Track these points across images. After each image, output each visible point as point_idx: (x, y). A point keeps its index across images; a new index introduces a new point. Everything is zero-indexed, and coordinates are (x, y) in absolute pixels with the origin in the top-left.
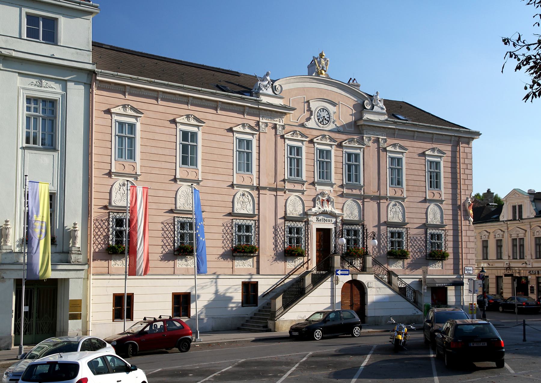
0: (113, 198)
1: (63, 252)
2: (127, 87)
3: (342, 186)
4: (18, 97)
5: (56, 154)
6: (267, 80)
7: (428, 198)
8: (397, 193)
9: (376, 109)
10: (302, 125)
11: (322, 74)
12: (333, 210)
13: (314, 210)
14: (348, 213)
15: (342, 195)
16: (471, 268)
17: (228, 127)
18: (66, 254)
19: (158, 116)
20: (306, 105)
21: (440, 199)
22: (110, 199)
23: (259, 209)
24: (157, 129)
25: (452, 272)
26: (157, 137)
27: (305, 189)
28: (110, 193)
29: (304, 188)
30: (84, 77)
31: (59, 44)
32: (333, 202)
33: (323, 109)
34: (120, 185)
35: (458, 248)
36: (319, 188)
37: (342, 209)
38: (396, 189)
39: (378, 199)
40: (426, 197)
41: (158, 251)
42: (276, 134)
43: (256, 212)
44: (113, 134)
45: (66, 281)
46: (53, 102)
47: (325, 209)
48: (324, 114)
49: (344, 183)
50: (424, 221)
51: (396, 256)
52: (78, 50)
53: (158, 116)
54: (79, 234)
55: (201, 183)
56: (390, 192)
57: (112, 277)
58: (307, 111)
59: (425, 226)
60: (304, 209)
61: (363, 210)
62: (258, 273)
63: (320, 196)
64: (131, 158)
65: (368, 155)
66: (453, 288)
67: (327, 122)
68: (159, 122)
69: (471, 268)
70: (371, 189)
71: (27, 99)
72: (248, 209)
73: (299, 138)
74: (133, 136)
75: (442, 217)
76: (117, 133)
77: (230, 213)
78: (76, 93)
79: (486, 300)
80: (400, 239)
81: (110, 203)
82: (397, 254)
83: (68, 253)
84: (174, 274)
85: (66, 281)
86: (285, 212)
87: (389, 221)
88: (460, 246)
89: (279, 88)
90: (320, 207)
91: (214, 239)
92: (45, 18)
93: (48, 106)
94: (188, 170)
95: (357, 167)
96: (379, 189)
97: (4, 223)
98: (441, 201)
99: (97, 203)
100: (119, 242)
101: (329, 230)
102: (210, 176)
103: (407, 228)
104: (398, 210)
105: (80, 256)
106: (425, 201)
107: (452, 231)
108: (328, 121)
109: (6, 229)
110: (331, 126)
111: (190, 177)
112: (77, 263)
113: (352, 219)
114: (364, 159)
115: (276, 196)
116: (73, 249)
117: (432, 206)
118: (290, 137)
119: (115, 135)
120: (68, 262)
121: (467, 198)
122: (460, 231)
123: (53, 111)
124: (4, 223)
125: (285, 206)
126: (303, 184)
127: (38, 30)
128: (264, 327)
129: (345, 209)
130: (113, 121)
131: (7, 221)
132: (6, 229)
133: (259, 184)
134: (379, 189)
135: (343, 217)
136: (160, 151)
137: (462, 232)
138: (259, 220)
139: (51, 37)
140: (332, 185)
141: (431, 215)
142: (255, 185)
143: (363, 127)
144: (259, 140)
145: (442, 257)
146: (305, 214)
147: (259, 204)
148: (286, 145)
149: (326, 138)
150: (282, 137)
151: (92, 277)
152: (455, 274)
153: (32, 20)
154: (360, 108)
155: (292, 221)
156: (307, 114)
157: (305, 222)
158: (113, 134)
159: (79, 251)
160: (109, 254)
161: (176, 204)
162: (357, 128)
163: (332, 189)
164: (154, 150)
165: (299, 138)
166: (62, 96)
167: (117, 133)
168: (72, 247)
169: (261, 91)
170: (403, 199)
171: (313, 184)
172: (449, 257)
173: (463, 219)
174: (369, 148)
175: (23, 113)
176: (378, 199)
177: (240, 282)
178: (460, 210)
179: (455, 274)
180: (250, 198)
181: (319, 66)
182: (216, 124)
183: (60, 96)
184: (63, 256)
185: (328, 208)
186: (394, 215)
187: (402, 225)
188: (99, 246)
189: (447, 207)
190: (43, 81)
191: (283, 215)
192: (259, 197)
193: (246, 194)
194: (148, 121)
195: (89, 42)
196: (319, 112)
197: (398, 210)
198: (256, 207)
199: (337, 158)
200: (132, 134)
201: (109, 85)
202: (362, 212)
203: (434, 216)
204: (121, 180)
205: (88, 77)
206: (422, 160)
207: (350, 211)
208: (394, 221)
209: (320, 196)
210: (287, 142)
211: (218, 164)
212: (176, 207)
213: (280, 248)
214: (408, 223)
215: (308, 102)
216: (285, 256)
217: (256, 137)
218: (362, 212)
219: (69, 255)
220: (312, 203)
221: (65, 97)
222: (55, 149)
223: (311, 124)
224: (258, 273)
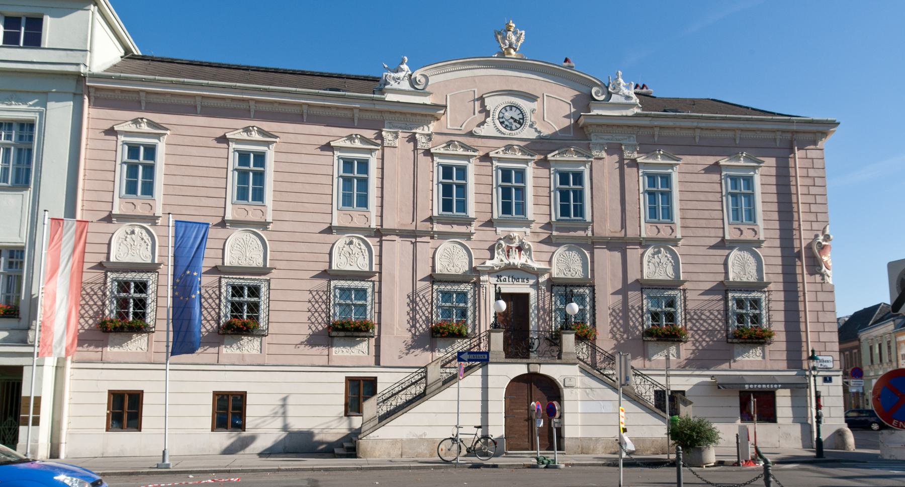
2: (141, 94)
3: (548, 226)
6: (402, 70)
7: (727, 237)
8: (662, 232)
9: (614, 99)
10: (471, 134)
11: (510, 54)
12: (530, 263)
13: (489, 263)
14: (562, 268)
15: (548, 241)
16: (830, 358)
17: (324, 143)
19: (198, 132)
20: (477, 104)
21: (756, 238)
23: (380, 264)
24: (195, 151)
25: (784, 365)
26: (193, 161)
27: (473, 231)
29: (472, 229)
30: (71, 86)
32: (529, 249)
33: (511, 107)
35: (799, 322)
36: (501, 231)
37: (550, 262)
38: (658, 225)
39: (619, 245)
40: (724, 237)
42: (415, 148)
43: (375, 268)
46: (31, 125)
47: (512, 261)
48: (516, 114)
49: (553, 219)
50: (721, 278)
51: (657, 336)
53: (198, 132)
55: (270, 227)
56: (647, 231)
57: (222, 368)
58: (480, 112)
59: (723, 288)
60: (471, 262)
61: (592, 262)
62: (378, 363)
63: (502, 242)
64: (750, 220)
65: (601, 174)
66: (787, 392)
67: (518, 126)
68: (198, 141)
69: (830, 358)
70: (609, 227)
72: (361, 263)
73: (460, 151)
74: (750, 192)
75: (759, 270)
76: (730, 190)
77: (325, 271)
79: (668, 416)
80: (143, 295)
82: (665, 333)
84: (218, 364)
86: (433, 267)
87: (645, 277)
88: (802, 320)
89: (423, 80)
90: (504, 259)
91: (289, 309)
94: (247, 208)
95: (579, 195)
96: (623, 226)
98: (758, 243)
100: (122, 315)
101: (526, 296)
102: (287, 216)
103: (684, 290)
104: (664, 260)
106: (723, 244)
107: (782, 293)
108: (521, 125)
110: (527, 133)
111: (251, 217)
113: (570, 276)
114: (591, 179)
115: (414, 244)
117: (735, 254)
118: (442, 151)
121: (817, 236)
122: (801, 294)
125: (433, 258)
126: (470, 225)
128: (348, 449)
129: (554, 260)
133: (382, 226)
134: (623, 226)
135: (551, 274)
136: (199, 182)
137: (804, 294)
138: (380, 281)
139: (34, 41)
140: (528, 224)
141: (736, 268)
142: (373, 225)
143: (590, 128)
144: (383, 159)
145: (760, 339)
146: (474, 271)
147: (380, 256)
148: (435, 165)
149: (514, 150)
150: (427, 153)
152: (790, 367)
154: (584, 101)
155: (143, 272)
156: (480, 117)
157: (474, 283)
161: (223, 258)
162: (580, 133)
163: (528, 230)
164: (187, 181)
165: (460, 151)
167: (341, 173)
169: (387, 87)
170: (675, 242)
171: (490, 223)
172: (775, 338)
173: (805, 272)
174: (601, 162)
176: (619, 245)
177: (342, 378)
178: (801, 260)
179: (790, 367)
180: (363, 247)
181: (505, 44)
182: (301, 139)
183: (37, 115)
184: (18, 335)
185: (518, 260)
186: (654, 267)
187: (675, 284)
188: (91, 322)
189: (771, 254)
191: (428, 272)
192: (381, 246)
193: (355, 240)
194: (285, 148)
196: (503, 111)
197: (664, 260)
198: (375, 260)
199: (537, 183)
200: (749, 189)
201: (112, 94)
202: (589, 266)
203: (741, 268)
204: (125, 227)
206: (326, 158)
207: (565, 264)
208: (657, 278)
209: (502, 242)
210: (495, 163)
211: (304, 198)
212: (223, 263)
213: (422, 327)
214: (685, 281)
215: (482, 99)
216: (433, 336)
217: (378, 153)
218: (589, 266)
220: (488, 254)
223: (488, 129)
224: (378, 363)
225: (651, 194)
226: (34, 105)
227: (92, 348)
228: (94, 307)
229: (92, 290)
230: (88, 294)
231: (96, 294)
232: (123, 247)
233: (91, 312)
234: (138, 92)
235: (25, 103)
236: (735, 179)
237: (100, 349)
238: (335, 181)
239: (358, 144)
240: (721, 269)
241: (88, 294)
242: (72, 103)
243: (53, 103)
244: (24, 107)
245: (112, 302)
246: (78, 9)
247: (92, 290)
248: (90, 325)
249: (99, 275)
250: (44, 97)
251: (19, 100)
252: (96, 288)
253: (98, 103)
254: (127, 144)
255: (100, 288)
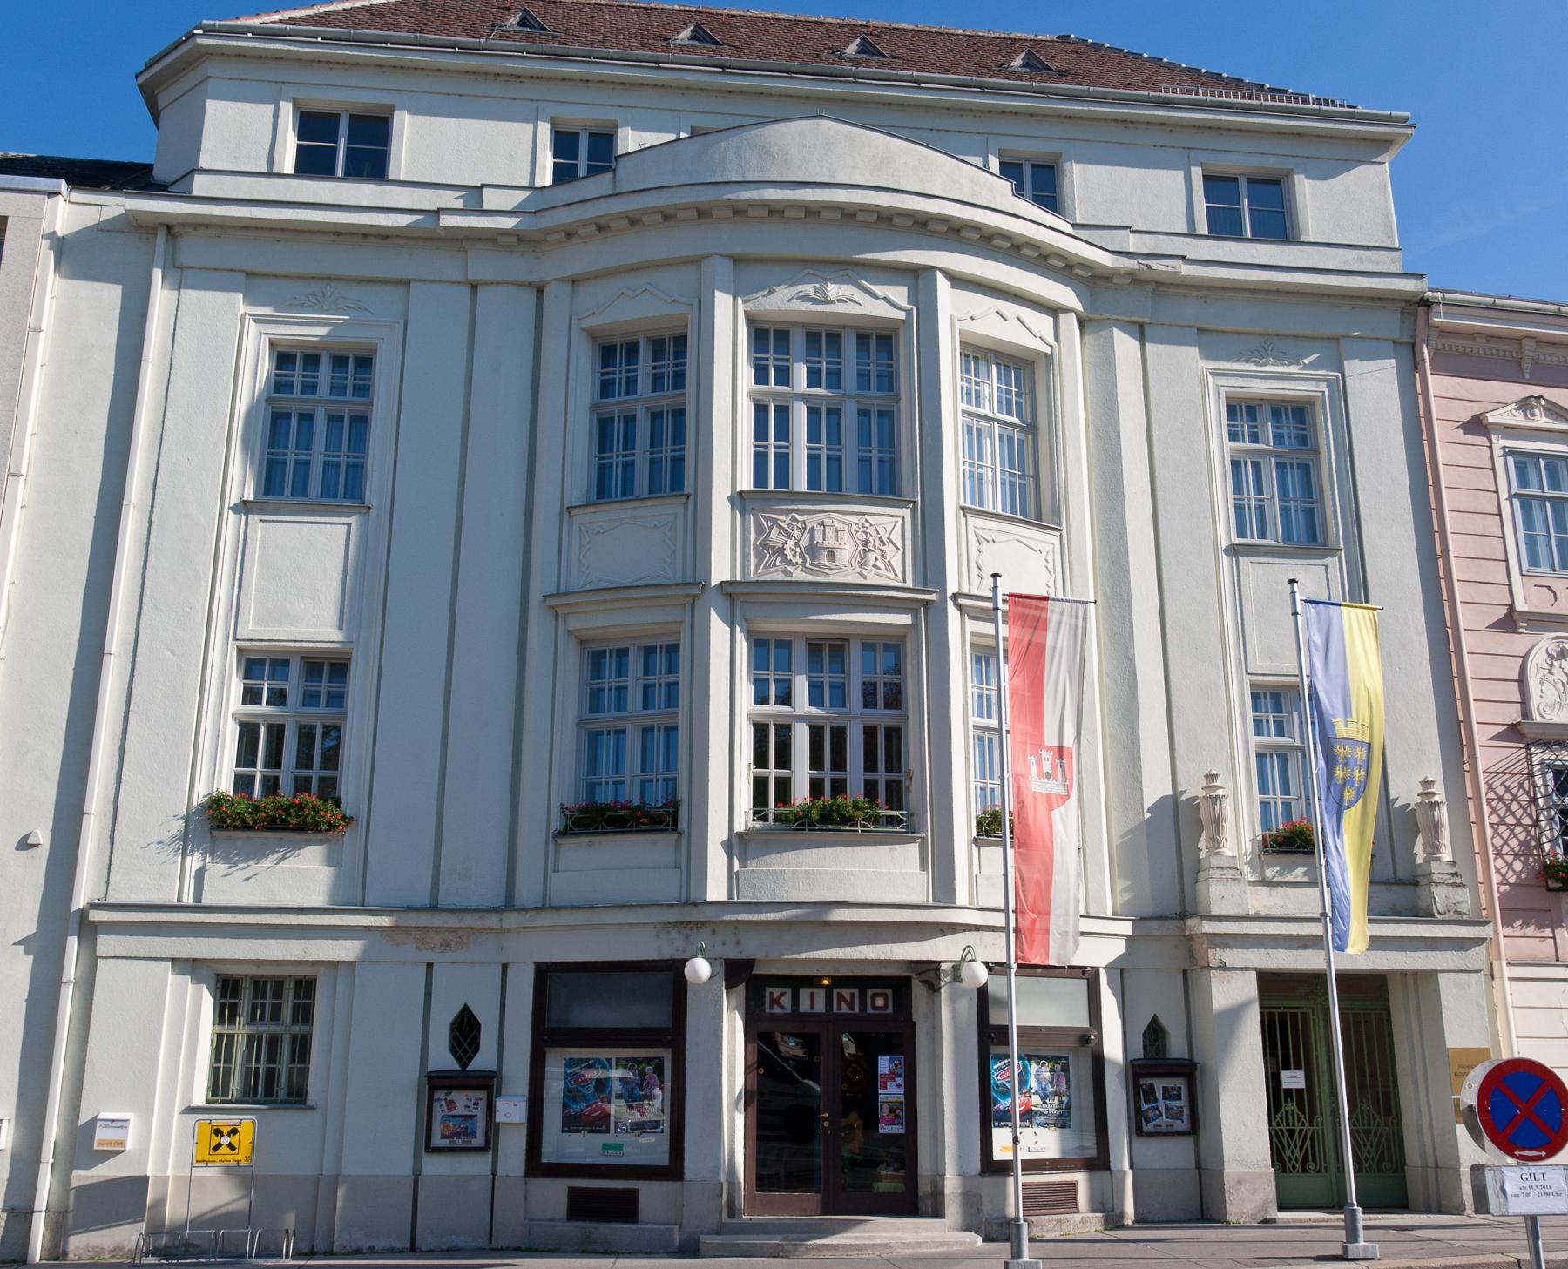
0: (1535, 700)
1: (1397, 882)
4: (1204, 398)
5: (1332, 562)
7: (1520, 606)
18: (1411, 888)
22: (1525, 703)
28: (1522, 681)
30: (1390, 325)
31: (1303, 238)
34: (1550, 656)
40: (1511, 607)
41: (1502, 872)
44: (1504, 494)
45: (1425, 980)
52: (1362, 252)
54: (1443, 814)
71: (1228, 406)
78: (1373, 385)
81: (1526, 714)
83: (1416, 883)
85: (1425, 980)
92: (1238, 236)
93: (1290, 428)
97: (1204, 783)
99: (1488, 715)
105: (1461, 891)
109: (1215, 800)
112: (1455, 917)
116: (1434, 866)
119: (1511, 497)
120: (1422, 913)
123: (1303, 440)
124: (1204, 783)
127: (1239, 212)
130: (1497, 453)
131: (1212, 777)
132: (1215, 800)
139: (1277, 223)
151: (1508, 972)
153: (1217, 185)
158: (1504, 494)
159: (1455, 874)
160: (1549, 890)
166: (1330, 383)
168: (1427, 861)
175: (1220, 449)
183: (1323, 386)
184: (1398, 895)
188: (1518, 866)
190: (900, 1080)
195: (1389, 226)
205: (1402, 322)
219: (1421, 890)
221: (1339, 389)
222: (1327, 550)
225: (1526, 501)
226: (1312, 365)
227: (1530, 930)
228: (1518, 829)
229: (1508, 790)
230: (1500, 799)
231: (1515, 799)
232: (1548, 688)
233: (1514, 843)
234: (1518, 340)
235: (1294, 360)
236: (1524, 462)
237: (1548, 932)
238: (1505, 505)
239: (1542, 421)
240: (1513, 693)
241: (1500, 799)
242: (1393, 362)
243: (1356, 362)
244: (1294, 369)
245: (1550, 819)
246: (1360, 162)
247: (1508, 790)
248: (1518, 874)
249: (1511, 754)
250: (1335, 350)
251: (1280, 358)
252: (1513, 783)
253: (1451, 365)
254: (1511, 453)
255: (1521, 786)
